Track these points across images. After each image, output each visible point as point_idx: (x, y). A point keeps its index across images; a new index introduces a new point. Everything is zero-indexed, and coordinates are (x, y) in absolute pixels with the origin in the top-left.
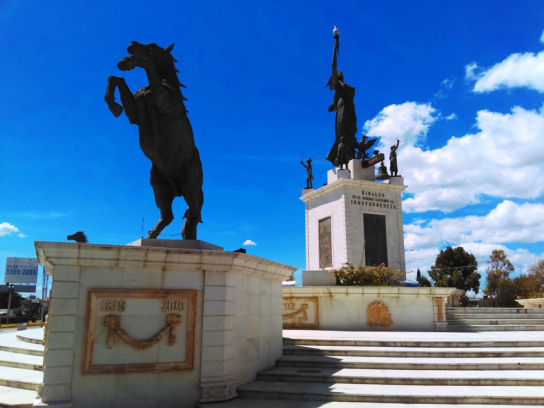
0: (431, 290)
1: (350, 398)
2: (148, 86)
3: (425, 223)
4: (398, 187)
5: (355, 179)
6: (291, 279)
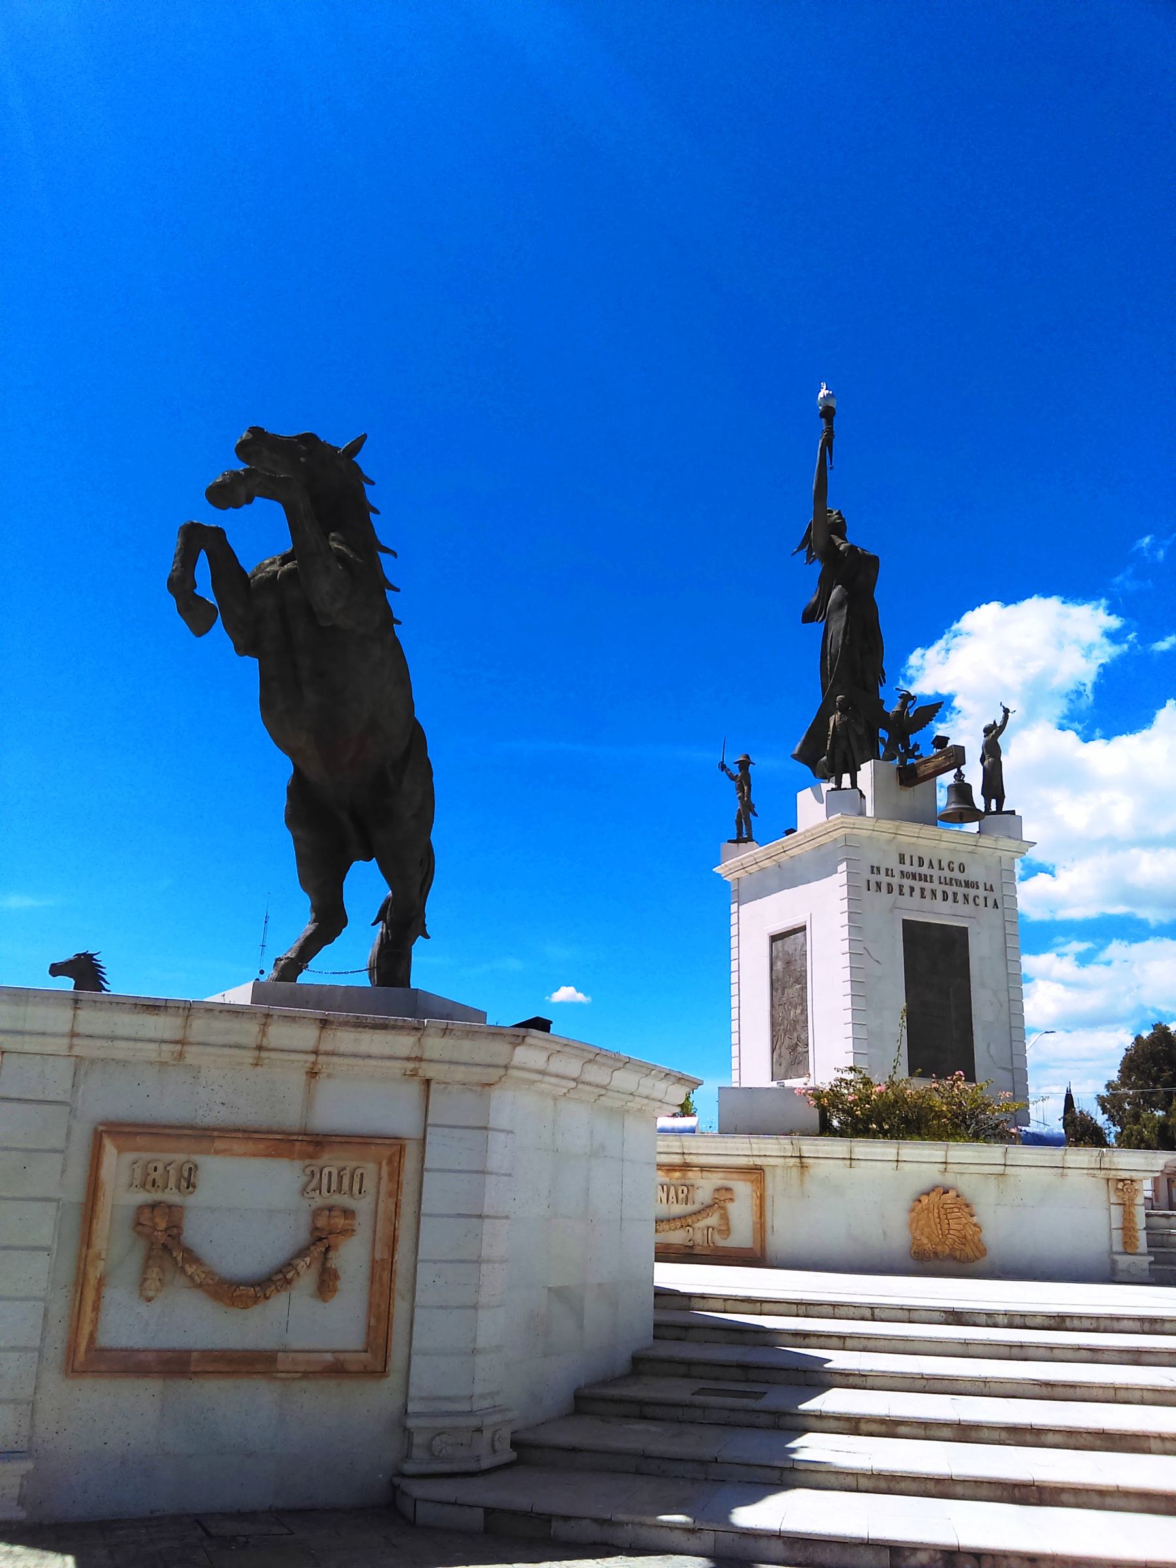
0: (1102, 1156)
1: (850, 1481)
2: (289, 549)
3: (1089, 950)
4: (1005, 843)
5: (877, 817)
6: (685, 1110)
